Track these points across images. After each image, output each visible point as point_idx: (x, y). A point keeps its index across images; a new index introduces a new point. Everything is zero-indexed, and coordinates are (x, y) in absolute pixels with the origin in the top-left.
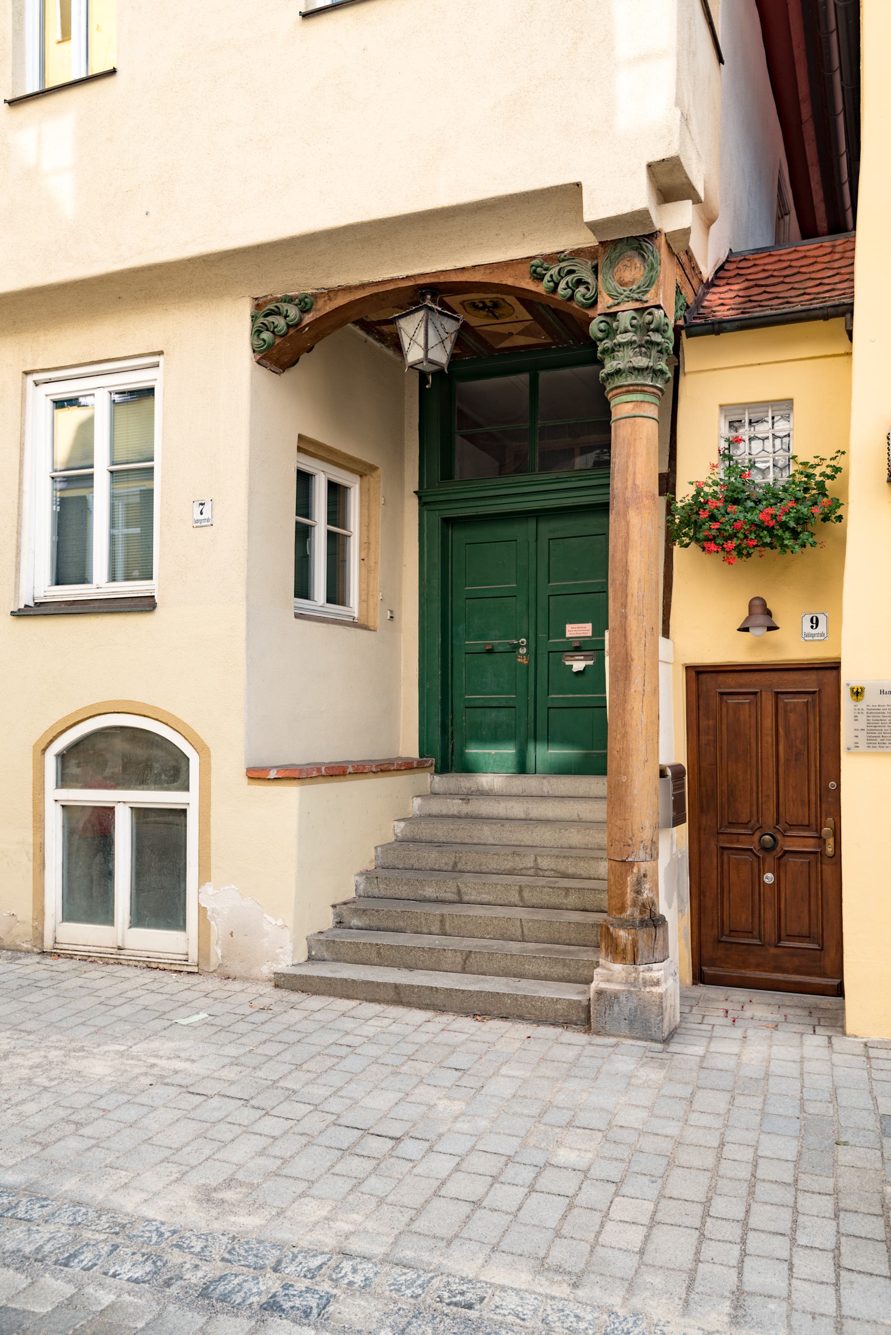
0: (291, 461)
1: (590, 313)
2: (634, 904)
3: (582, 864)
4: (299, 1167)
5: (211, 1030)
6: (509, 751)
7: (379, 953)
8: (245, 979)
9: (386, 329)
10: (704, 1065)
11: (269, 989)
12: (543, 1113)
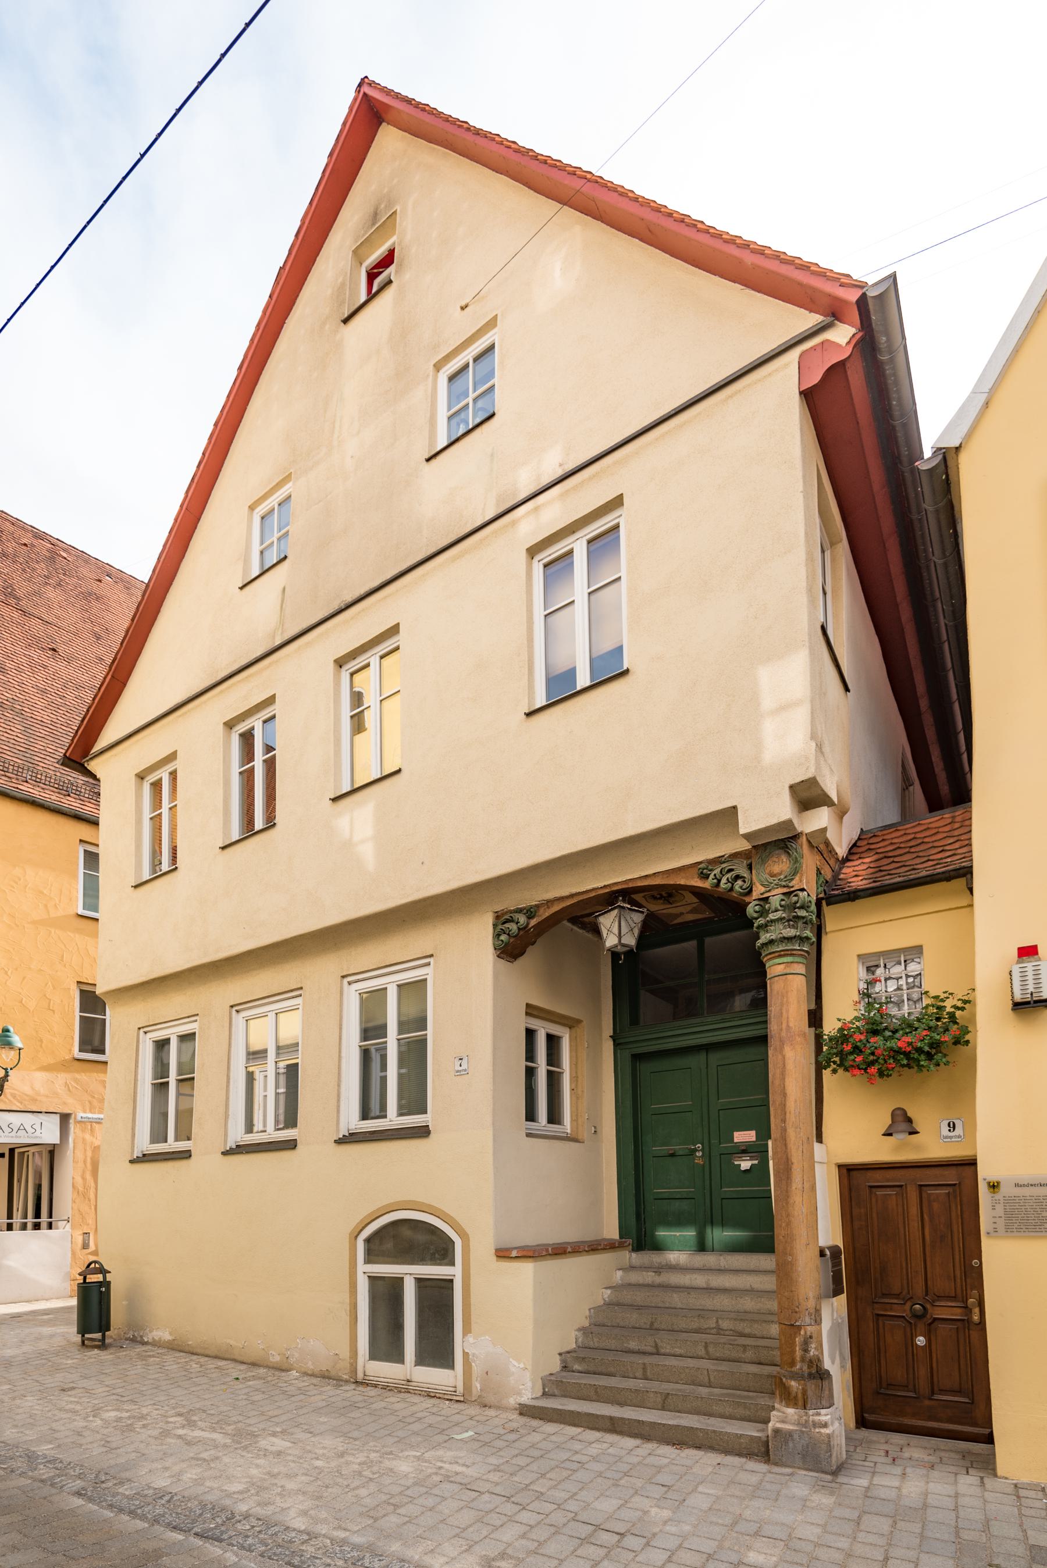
0: (521, 1022)
1: (747, 899)
2: (803, 1360)
3: (756, 1326)
4: (552, 1548)
5: (477, 1445)
6: (690, 1233)
7: (596, 1392)
8: (498, 1408)
9: (586, 920)
10: (869, 1494)
11: (515, 1416)
12: (735, 1523)
